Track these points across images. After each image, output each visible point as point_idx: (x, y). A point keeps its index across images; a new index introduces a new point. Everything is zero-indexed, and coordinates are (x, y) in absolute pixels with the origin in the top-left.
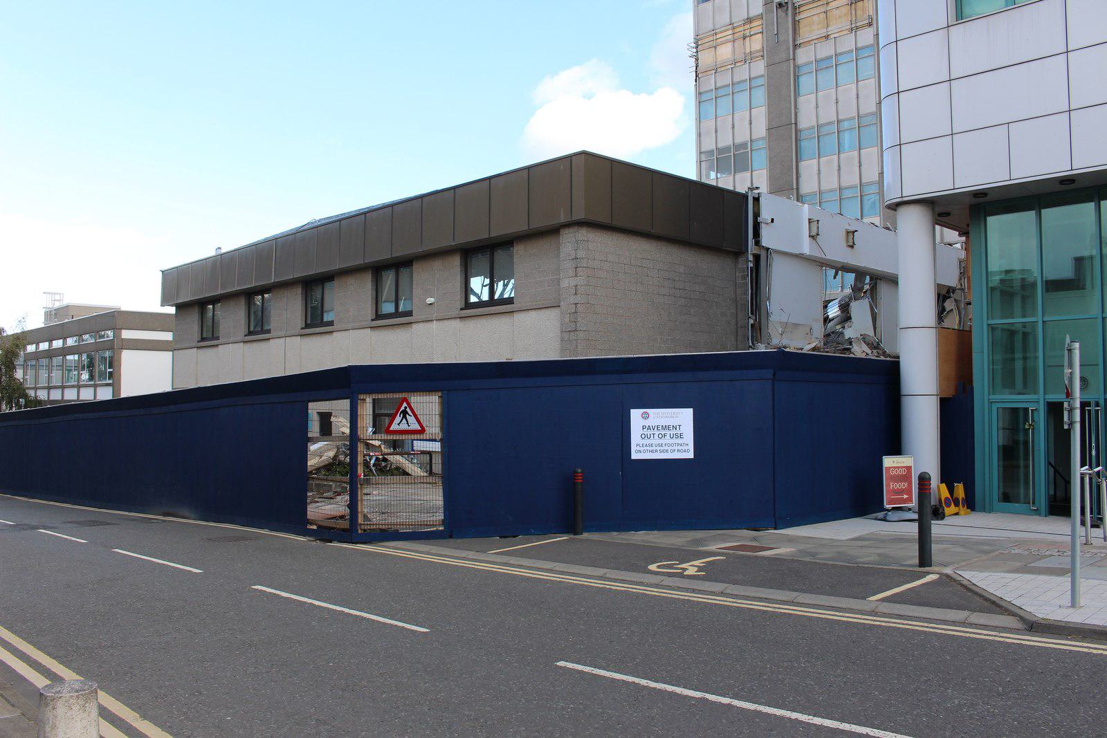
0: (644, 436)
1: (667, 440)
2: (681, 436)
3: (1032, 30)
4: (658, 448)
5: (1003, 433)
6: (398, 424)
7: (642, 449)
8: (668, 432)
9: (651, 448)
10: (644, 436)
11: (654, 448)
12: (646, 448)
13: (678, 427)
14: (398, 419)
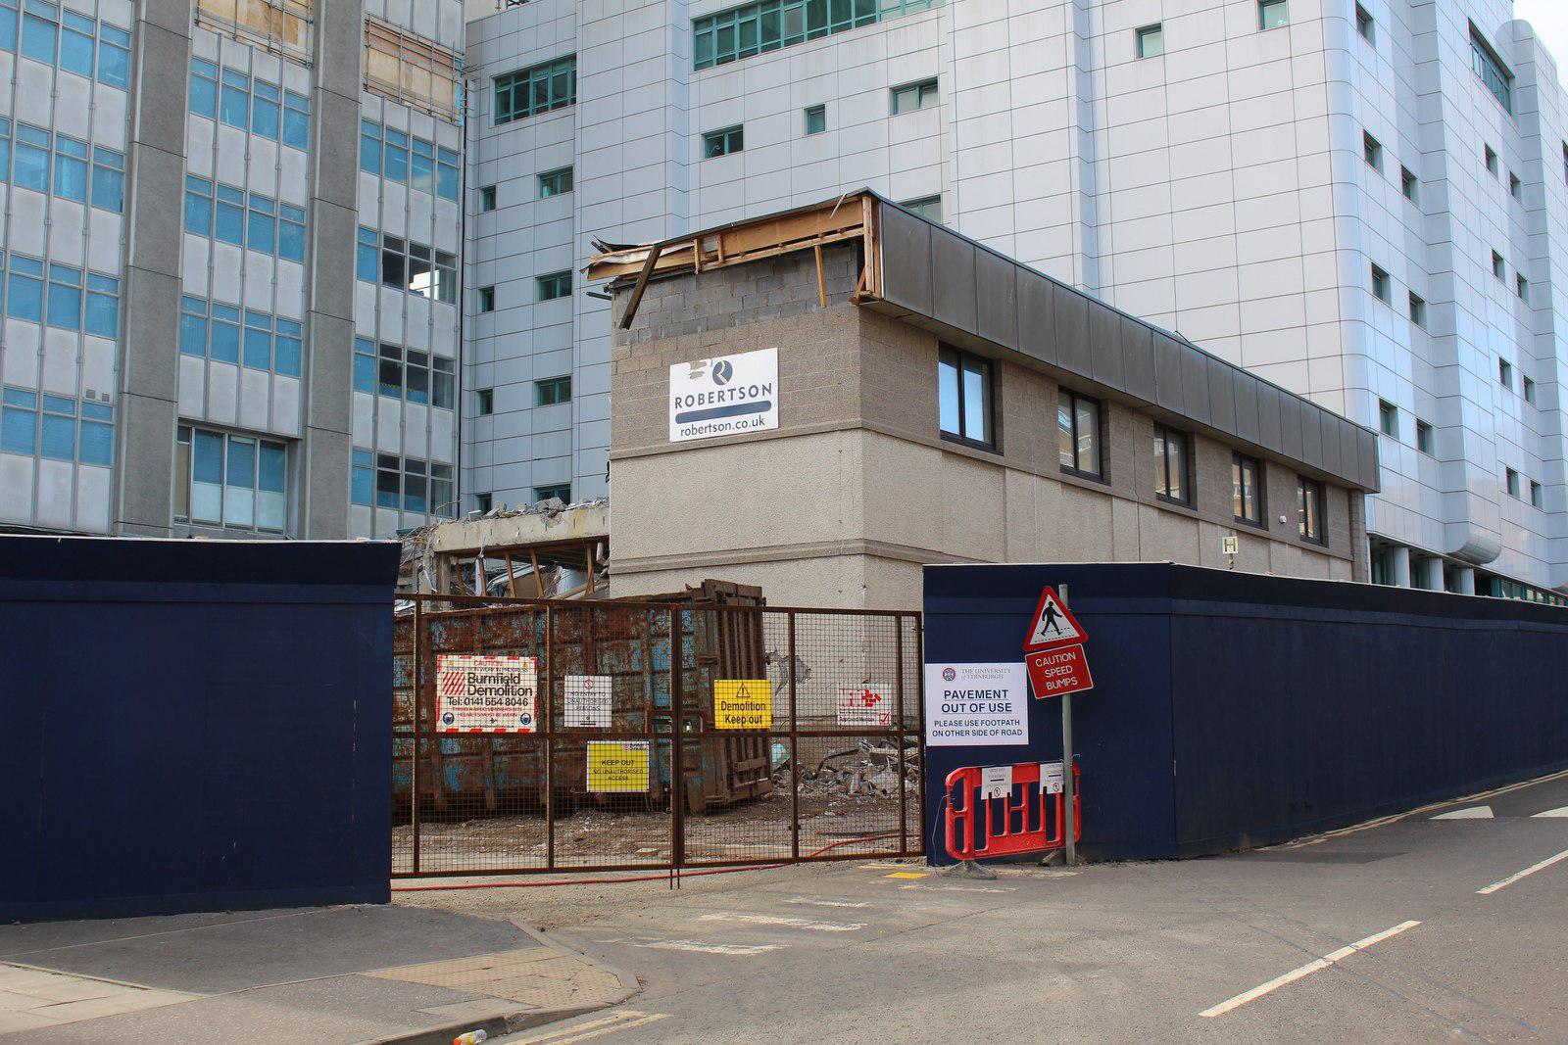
0: (947, 709)
1: (985, 715)
2: (1007, 708)
3: (848, 65)
4: (970, 728)
5: (441, 846)
6: (1043, 633)
7: (944, 729)
8: (987, 702)
9: (958, 729)
10: (947, 709)
11: (965, 728)
12: (951, 728)
13: (1002, 694)
14: (1041, 624)
